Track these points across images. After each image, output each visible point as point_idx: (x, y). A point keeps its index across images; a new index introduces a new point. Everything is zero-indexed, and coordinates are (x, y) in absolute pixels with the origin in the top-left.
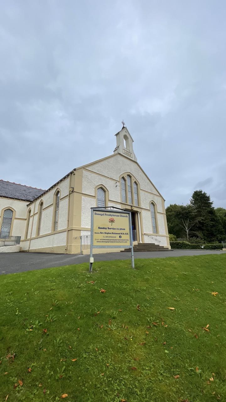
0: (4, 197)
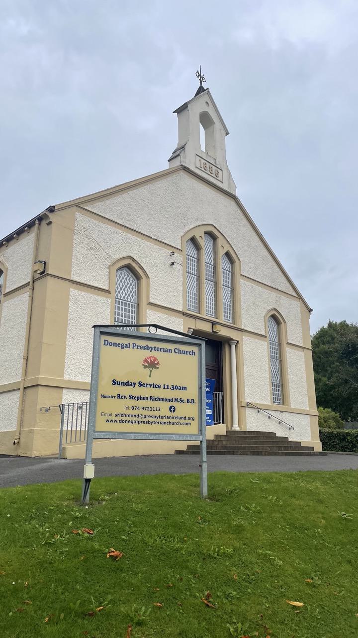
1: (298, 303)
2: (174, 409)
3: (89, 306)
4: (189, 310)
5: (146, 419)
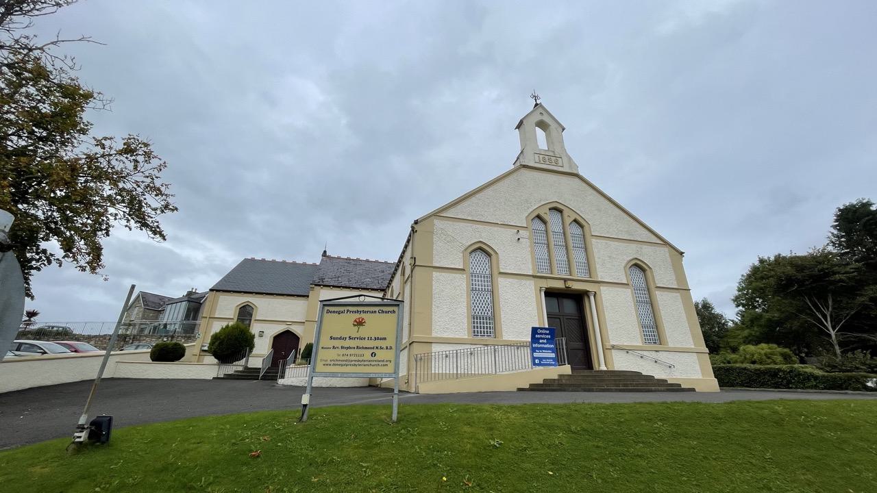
0: (344, 287)
1: (666, 249)
2: (375, 354)
3: (449, 282)
4: (538, 272)
5: (353, 363)
